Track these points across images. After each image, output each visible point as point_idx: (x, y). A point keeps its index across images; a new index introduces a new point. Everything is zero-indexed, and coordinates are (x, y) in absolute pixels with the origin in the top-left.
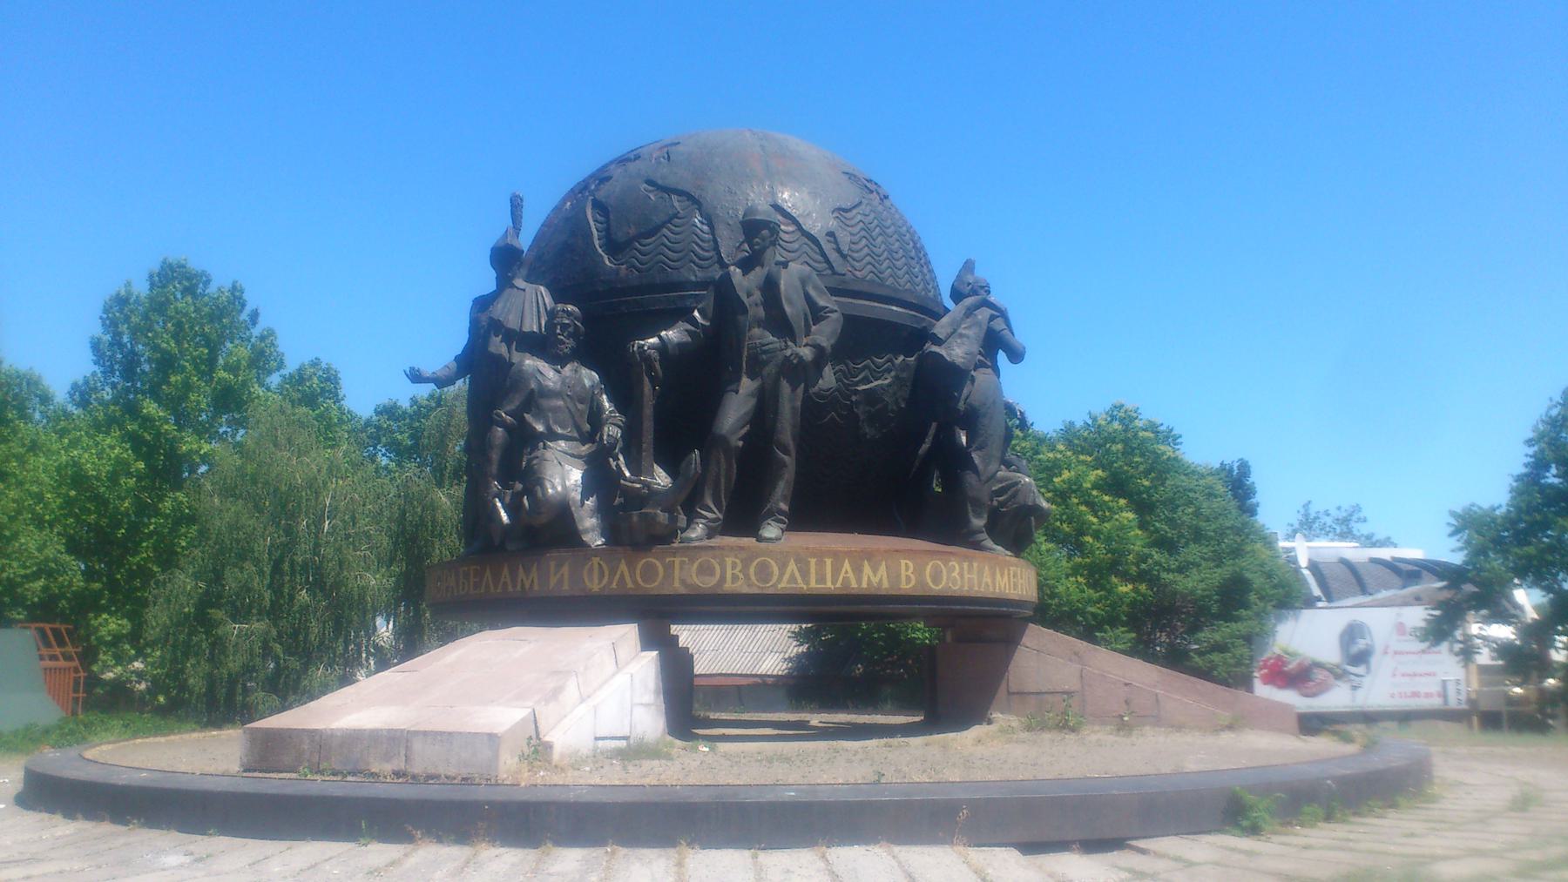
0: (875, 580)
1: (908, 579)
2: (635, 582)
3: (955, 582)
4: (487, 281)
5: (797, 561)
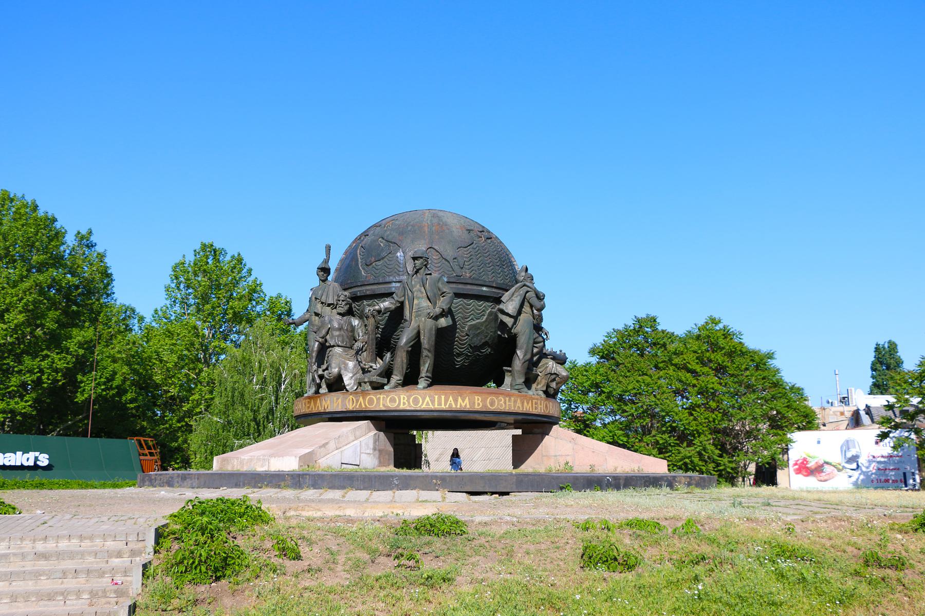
0: (463, 405)
1: (479, 404)
4: (315, 282)
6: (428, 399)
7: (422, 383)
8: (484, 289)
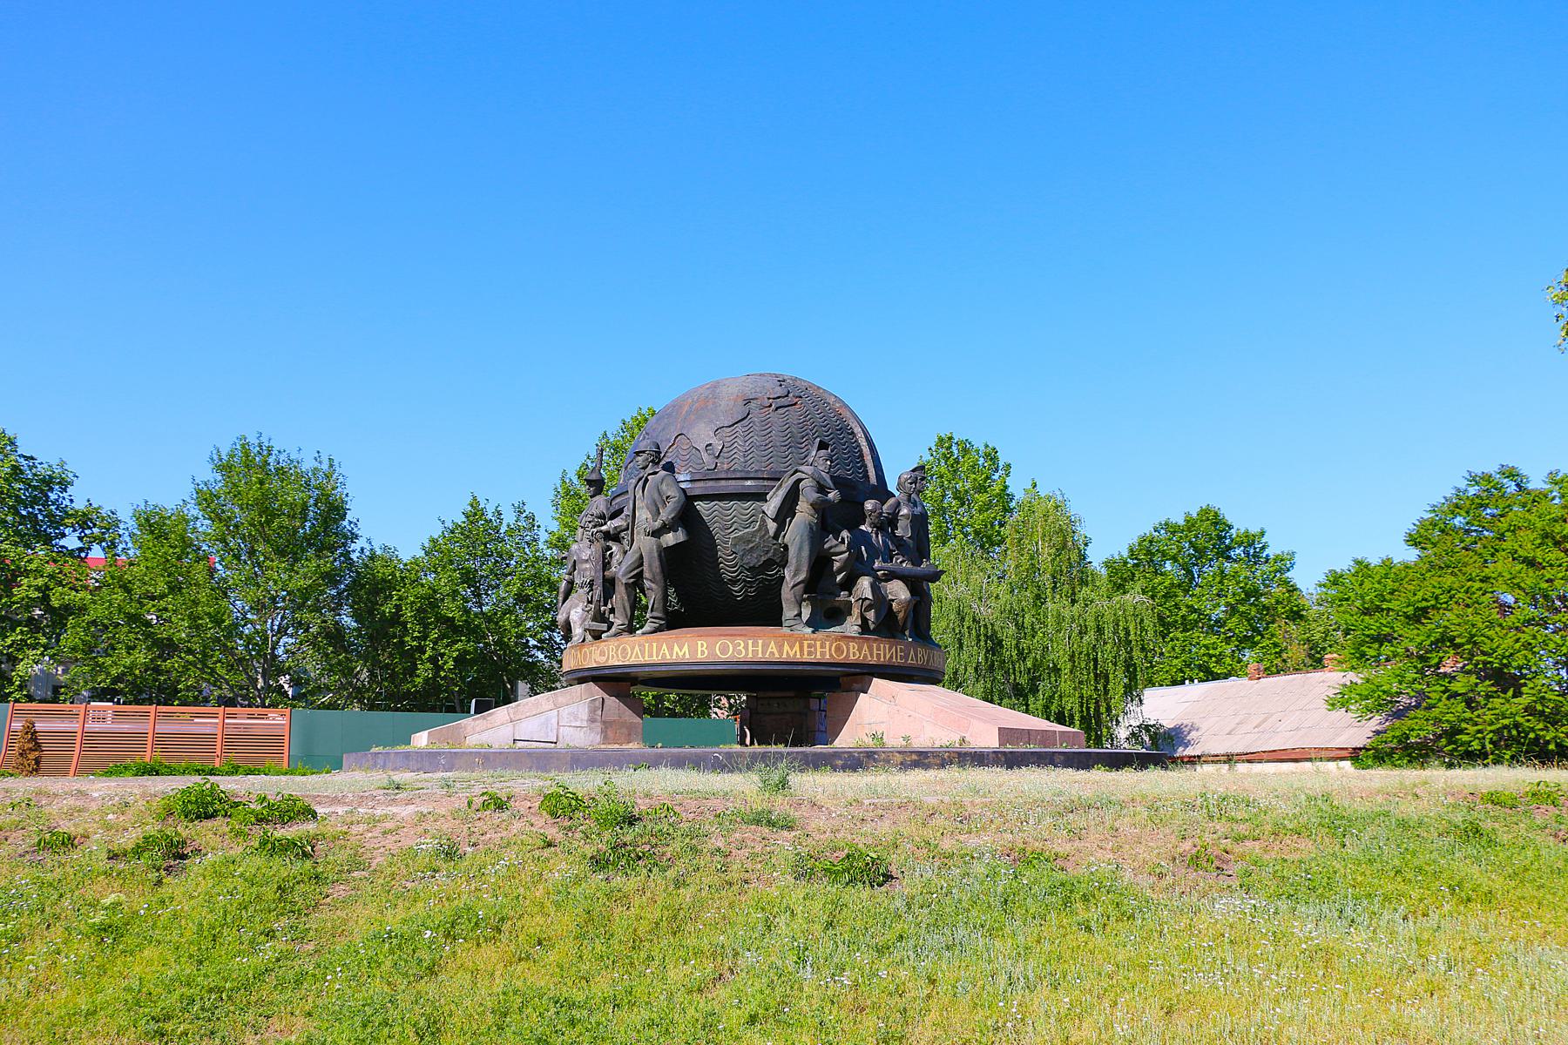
8: (749, 483)
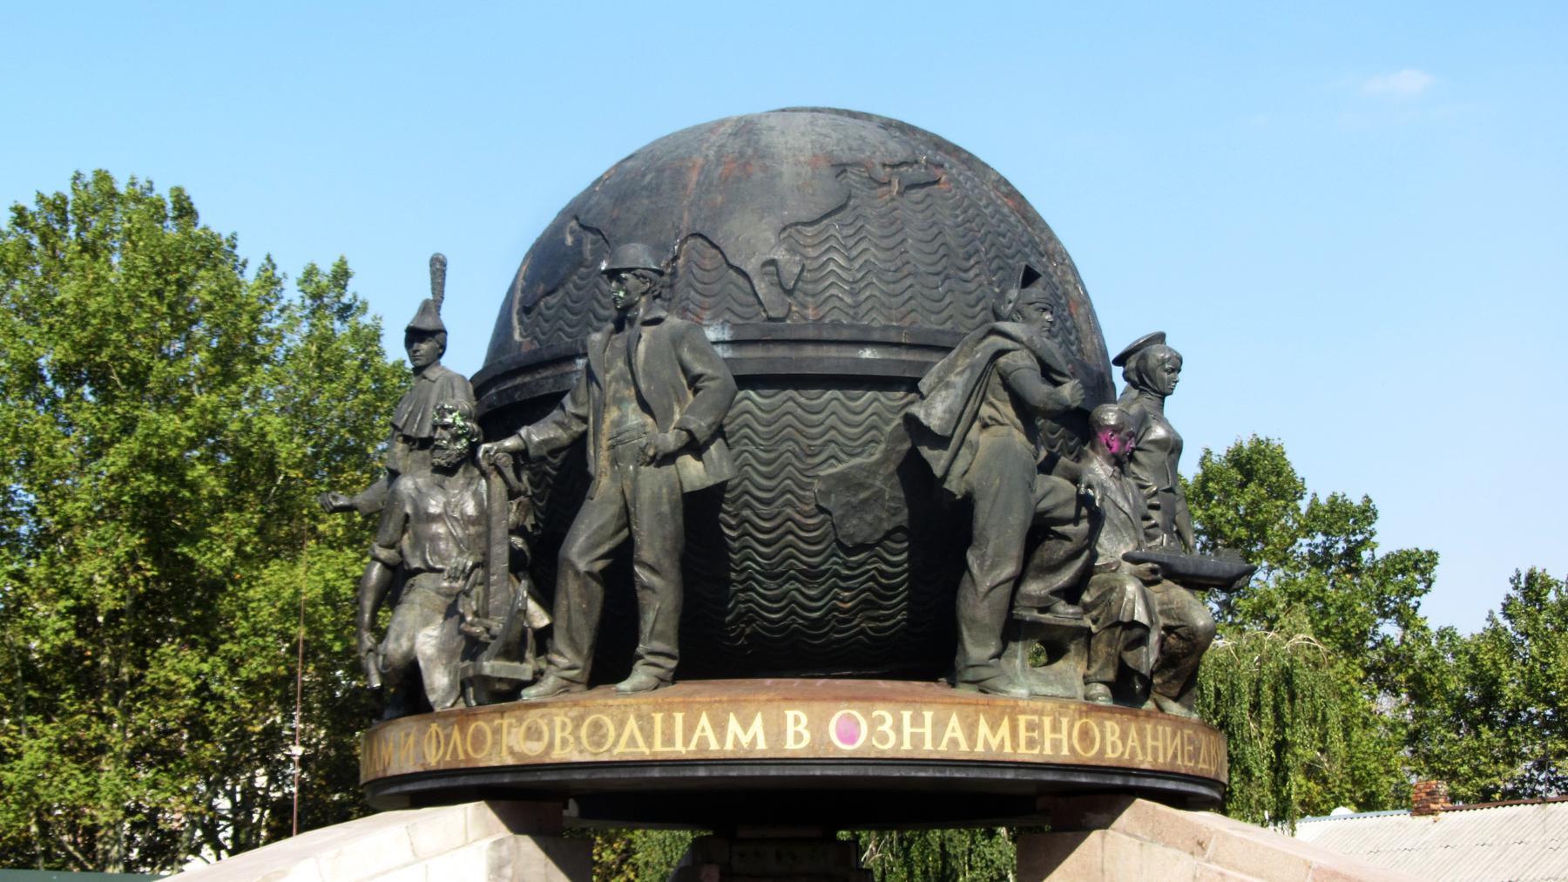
0: (994, 743)
1: (798, 737)
2: (466, 752)
3: (884, 738)
5: (639, 717)
6: (632, 724)
7: (641, 675)
8: (867, 353)
